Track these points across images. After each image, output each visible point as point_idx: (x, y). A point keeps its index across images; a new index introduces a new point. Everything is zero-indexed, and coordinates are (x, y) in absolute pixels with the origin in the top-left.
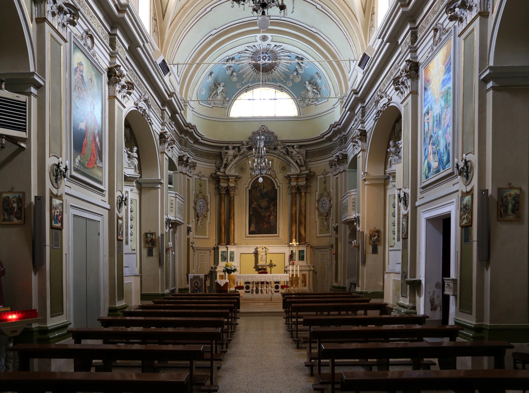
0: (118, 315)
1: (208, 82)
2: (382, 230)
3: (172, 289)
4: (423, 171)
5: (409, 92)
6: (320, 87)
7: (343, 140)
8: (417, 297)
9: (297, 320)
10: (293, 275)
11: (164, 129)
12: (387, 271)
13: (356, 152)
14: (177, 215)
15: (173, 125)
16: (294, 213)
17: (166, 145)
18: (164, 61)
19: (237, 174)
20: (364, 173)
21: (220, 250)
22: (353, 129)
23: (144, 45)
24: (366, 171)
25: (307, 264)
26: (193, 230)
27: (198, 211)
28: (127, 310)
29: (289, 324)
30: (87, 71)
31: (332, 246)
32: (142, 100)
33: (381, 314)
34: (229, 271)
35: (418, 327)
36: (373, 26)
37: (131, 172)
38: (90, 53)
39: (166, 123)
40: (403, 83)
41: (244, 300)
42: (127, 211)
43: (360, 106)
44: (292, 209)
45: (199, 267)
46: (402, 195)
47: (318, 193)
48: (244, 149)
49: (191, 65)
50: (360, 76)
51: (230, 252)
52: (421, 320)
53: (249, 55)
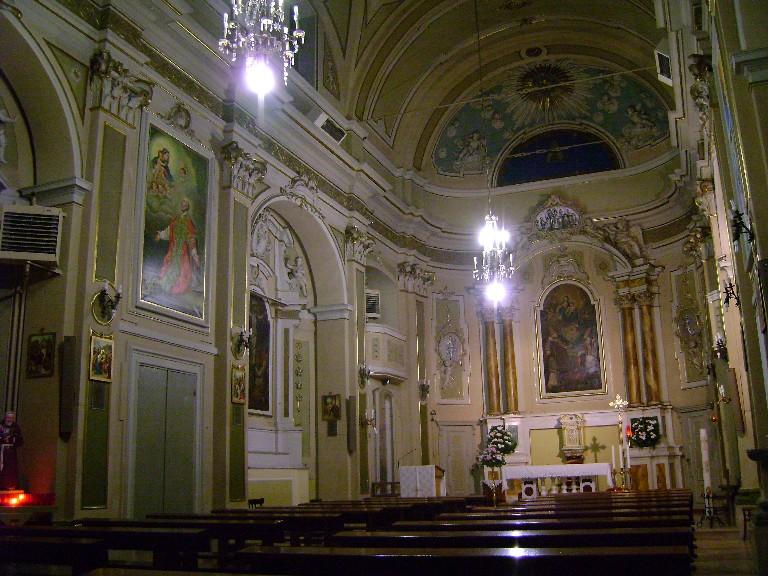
27: (444, 357)
44: (625, 340)
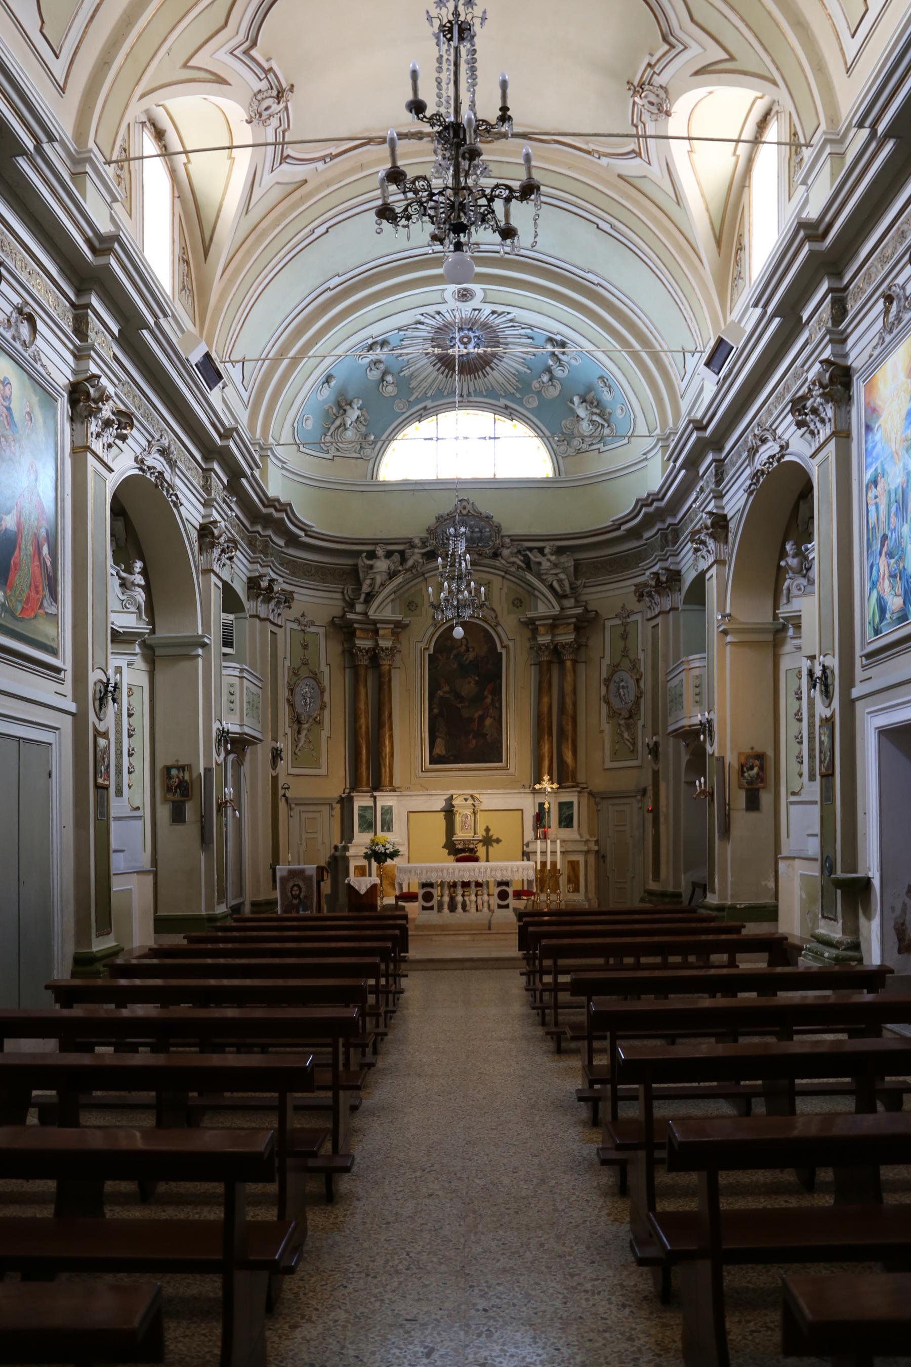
0: (97, 974)
1: (320, 398)
2: (770, 753)
3: (234, 902)
4: (868, 617)
5: (828, 432)
6: (609, 410)
7: (670, 537)
8: (862, 920)
9: (555, 979)
10: (544, 864)
11: (210, 515)
12: (785, 852)
13: (703, 565)
14: (246, 720)
15: (233, 505)
16: (546, 710)
17: (216, 553)
18: (207, 356)
19: (399, 617)
20: (723, 617)
21: (357, 804)
22: (694, 511)
23: (157, 324)
24: (728, 611)
25: (580, 834)
26: (287, 755)
27: (299, 710)
28: (119, 961)
29: (534, 990)
30: (21, 397)
31: (644, 792)
32: (154, 449)
33: (771, 964)
34: (378, 856)
35: (866, 997)
36: (739, 276)
37: (127, 621)
38: (26, 355)
39: (215, 500)
40: (815, 411)
41: (417, 927)
42: (119, 715)
43: (710, 457)
44: (539, 702)
45: (303, 848)
46: (818, 672)
47: (607, 661)
48: (415, 557)
49: (277, 361)
50: (710, 389)
51: (383, 807)
52: (874, 979)
53: (425, 334)
